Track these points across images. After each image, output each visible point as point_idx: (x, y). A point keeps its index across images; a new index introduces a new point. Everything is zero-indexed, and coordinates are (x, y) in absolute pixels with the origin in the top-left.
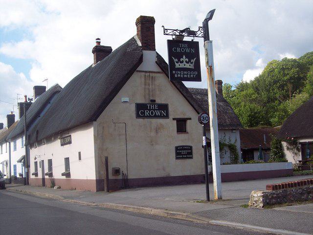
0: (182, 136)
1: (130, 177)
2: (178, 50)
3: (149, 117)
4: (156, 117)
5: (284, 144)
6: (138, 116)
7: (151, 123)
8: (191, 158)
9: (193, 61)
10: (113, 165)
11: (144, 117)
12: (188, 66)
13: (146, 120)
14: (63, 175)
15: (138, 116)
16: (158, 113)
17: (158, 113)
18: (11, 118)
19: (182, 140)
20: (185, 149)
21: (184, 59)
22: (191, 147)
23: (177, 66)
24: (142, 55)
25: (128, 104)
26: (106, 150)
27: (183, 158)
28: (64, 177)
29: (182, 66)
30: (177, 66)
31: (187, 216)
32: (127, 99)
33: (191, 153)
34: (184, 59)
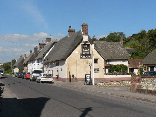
0: (96, 65)
1: (78, 78)
2: (84, 47)
3: (85, 58)
4: (87, 58)
5: (122, 70)
6: (81, 58)
7: (85, 60)
8: (99, 72)
9: (88, 49)
10: (71, 74)
11: (83, 58)
12: (87, 51)
13: (84, 59)
14: (56, 76)
15: (81, 58)
16: (88, 57)
17: (88, 57)
18: (31, 52)
19: (96, 66)
20: (97, 69)
21: (86, 49)
22: (99, 69)
23: (84, 51)
24: (83, 37)
25: (77, 54)
26: (70, 68)
27: (96, 72)
28: (56, 77)
29: (85, 51)
30: (84, 51)
31: (81, 88)
32: (77, 52)
33: (99, 71)
34: (86, 49)
